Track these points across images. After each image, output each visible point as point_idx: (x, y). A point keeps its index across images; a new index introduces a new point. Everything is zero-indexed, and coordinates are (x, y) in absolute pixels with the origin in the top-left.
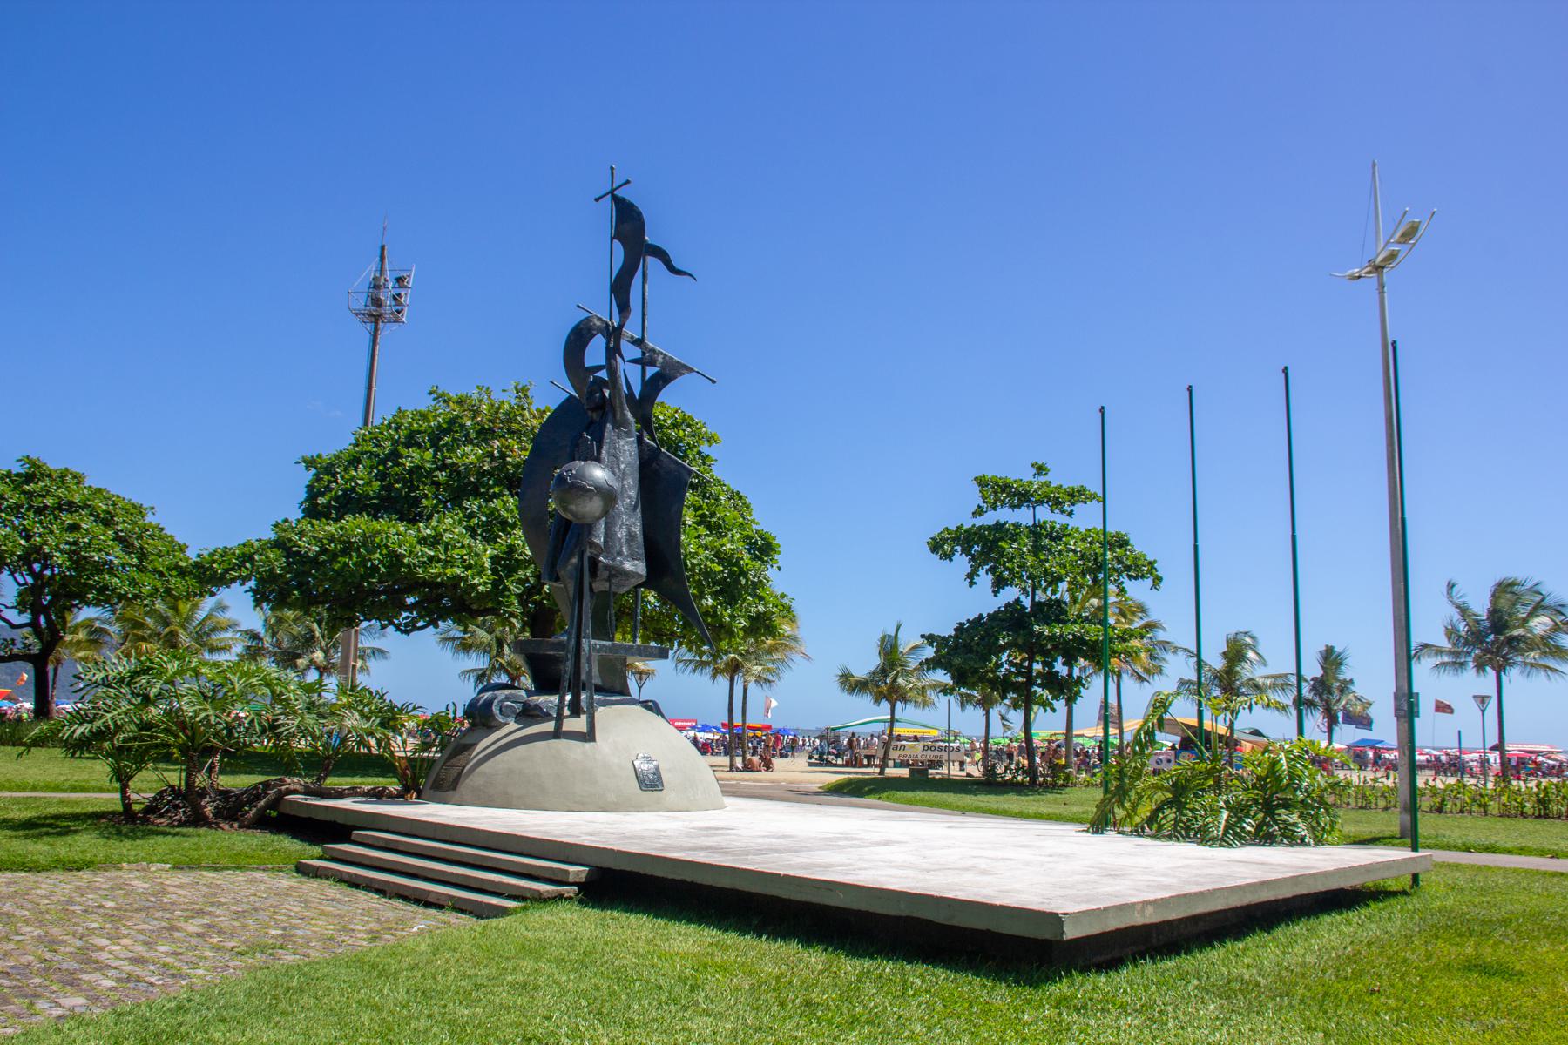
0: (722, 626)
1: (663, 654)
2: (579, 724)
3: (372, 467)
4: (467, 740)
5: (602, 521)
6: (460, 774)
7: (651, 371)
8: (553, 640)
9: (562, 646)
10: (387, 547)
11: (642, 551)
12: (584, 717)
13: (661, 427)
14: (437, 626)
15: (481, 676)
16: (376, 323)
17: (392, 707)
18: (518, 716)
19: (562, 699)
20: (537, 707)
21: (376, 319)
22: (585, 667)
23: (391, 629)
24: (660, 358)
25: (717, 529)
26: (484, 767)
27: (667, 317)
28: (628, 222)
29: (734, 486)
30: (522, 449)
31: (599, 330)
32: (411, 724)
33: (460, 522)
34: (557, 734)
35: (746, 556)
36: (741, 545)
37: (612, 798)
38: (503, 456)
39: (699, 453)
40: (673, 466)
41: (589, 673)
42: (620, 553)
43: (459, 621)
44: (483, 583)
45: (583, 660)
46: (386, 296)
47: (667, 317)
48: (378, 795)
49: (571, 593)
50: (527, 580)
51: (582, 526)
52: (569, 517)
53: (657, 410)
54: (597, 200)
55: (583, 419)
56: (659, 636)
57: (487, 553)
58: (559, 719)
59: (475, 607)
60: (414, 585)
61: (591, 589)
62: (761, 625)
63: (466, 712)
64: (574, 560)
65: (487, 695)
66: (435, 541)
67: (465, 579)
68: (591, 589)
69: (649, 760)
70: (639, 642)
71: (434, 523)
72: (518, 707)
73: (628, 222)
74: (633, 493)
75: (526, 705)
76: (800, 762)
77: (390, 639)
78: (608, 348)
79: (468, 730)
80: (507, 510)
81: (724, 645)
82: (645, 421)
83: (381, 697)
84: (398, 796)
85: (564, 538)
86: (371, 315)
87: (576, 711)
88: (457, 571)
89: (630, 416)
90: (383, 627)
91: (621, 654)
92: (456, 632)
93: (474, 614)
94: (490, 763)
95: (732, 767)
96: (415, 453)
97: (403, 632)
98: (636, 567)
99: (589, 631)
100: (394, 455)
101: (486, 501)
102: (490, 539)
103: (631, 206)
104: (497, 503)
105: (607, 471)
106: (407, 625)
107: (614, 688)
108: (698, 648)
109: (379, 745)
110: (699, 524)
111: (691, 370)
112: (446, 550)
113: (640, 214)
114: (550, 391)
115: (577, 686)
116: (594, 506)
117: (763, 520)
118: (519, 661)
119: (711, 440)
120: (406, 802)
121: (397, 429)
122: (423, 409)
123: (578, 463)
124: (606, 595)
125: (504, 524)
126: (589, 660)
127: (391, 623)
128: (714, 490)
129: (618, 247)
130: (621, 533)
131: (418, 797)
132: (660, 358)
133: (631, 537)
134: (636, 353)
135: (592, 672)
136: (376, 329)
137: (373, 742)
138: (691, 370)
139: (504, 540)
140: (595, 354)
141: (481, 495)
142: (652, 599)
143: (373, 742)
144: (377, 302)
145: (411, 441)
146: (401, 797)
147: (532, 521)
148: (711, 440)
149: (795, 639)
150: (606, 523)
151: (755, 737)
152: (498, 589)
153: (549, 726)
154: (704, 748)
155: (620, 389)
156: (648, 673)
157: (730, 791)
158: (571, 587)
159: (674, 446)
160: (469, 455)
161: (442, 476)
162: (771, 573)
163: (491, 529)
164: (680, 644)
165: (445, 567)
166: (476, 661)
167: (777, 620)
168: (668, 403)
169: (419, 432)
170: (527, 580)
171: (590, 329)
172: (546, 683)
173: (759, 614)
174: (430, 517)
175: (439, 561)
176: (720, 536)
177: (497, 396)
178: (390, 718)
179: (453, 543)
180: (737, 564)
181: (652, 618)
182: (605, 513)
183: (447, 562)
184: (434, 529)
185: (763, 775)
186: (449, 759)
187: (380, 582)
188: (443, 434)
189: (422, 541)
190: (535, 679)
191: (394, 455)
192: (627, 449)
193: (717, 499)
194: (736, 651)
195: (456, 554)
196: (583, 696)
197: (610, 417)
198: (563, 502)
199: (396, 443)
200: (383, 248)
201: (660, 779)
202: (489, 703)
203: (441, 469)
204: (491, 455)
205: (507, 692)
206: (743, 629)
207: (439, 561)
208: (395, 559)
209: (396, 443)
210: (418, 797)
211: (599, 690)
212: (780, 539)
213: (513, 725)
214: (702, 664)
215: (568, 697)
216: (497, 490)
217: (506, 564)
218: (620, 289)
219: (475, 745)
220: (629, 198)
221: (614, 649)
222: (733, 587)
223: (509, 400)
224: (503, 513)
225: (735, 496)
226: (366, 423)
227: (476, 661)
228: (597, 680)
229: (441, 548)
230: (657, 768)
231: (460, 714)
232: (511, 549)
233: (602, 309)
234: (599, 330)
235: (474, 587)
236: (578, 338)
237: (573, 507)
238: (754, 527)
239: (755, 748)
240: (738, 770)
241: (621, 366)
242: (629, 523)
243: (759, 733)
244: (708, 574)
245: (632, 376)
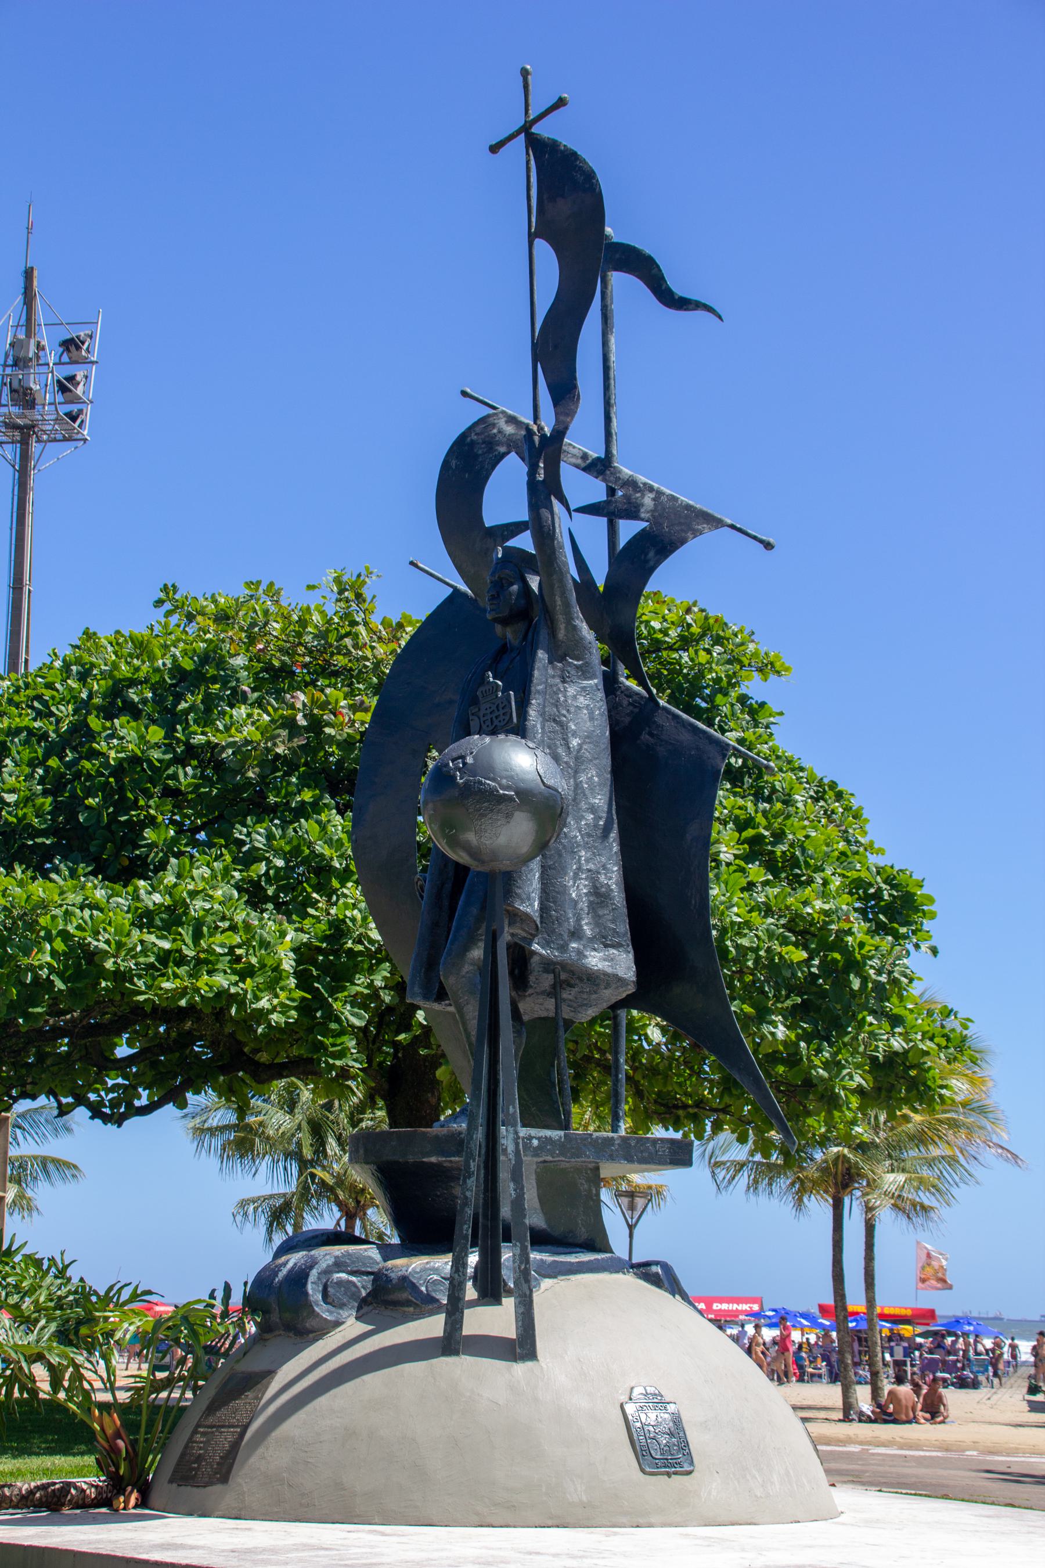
0: (809, 1084)
1: (679, 1155)
2: (496, 1320)
3: (32, 764)
4: (252, 1365)
5: (535, 865)
6: (235, 1446)
7: (628, 530)
8: (435, 1130)
9: (457, 1143)
10: (65, 935)
11: (623, 927)
12: (509, 1303)
13: (657, 646)
14: (182, 1105)
15: (280, 1213)
16: (25, 443)
17: (84, 1294)
18: (363, 1303)
19: (459, 1264)
20: (406, 1282)
21: (25, 434)
22: (507, 1189)
23: (82, 1113)
24: (648, 500)
25: (790, 869)
26: (291, 1426)
27: (662, 405)
28: (565, 195)
29: (823, 769)
30: (354, 708)
31: (512, 445)
32: (128, 1329)
33: (226, 872)
34: (451, 1343)
35: (859, 927)
36: (844, 903)
37: (577, 1492)
38: (316, 725)
39: (743, 699)
40: (685, 737)
41: (518, 1204)
42: (576, 934)
43: (229, 1092)
44: (276, 1006)
45: (504, 1174)
46: (41, 382)
47: (662, 405)
48: (52, 1503)
49: (473, 1024)
50: (375, 994)
51: (489, 878)
52: (462, 857)
53: (646, 607)
54: (494, 149)
55: (484, 645)
56: (669, 1111)
57: (286, 941)
58: (455, 1310)
59: (264, 1057)
60: (131, 1016)
61: (516, 1014)
62: (900, 1081)
63: (247, 1299)
64: (477, 953)
65: (294, 1259)
66: (172, 918)
67: (239, 1000)
68: (516, 1014)
69: (658, 1401)
70: (625, 1126)
71: (170, 879)
72: (363, 1285)
73: (565, 195)
74: (600, 800)
75: (380, 1279)
76: (1008, 1400)
77: (83, 1137)
78: (532, 485)
79: (255, 1341)
80: (329, 842)
81: (816, 1124)
82: (622, 643)
83: (61, 1273)
84: (98, 1503)
85: (453, 902)
86: (16, 427)
87: (491, 1290)
88: (221, 981)
89: (587, 633)
90: (63, 1111)
91: (588, 1158)
92: (224, 1116)
93: (264, 1074)
94: (301, 1415)
95: (849, 1412)
96: (126, 728)
97: (106, 1119)
98: (614, 962)
99: (515, 1109)
100: (80, 735)
101: (285, 824)
102: (294, 908)
103: (570, 159)
104: (308, 827)
105: (543, 755)
106: (114, 1104)
107: (574, 1236)
108: (760, 1132)
109: (56, 1383)
110: (748, 858)
111: (718, 523)
112: (197, 936)
113: (590, 176)
114: (410, 583)
115: (491, 1233)
116: (514, 833)
117: (893, 844)
118: (361, 1176)
119: (767, 668)
120: (117, 1516)
121: (83, 677)
122: (140, 630)
123: (477, 742)
124: (549, 1025)
125: (322, 872)
126: (517, 1176)
127: (81, 1100)
128: (780, 781)
129: (545, 252)
130: (577, 890)
131: (143, 1503)
132: (648, 500)
133: (599, 896)
134: (594, 490)
135: (525, 1200)
136: (25, 457)
137: (40, 1371)
138: (718, 523)
139: (322, 912)
140: (505, 496)
141: (273, 811)
142: (655, 1034)
143: (40, 1371)
144: (25, 398)
145: (116, 703)
146: (102, 1504)
147: (383, 867)
148: (767, 668)
149: (982, 1110)
150: (544, 869)
151: (894, 1337)
152: (314, 1012)
153: (433, 1326)
154: (783, 1364)
155: (562, 573)
156: (651, 1194)
157: (844, 1471)
158: (472, 1011)
159: (688, 690)
160: (244, 724)
161: (186, 776)
162: (917, 961)
163: (290, 889)
164: (717, 1127)
165: (194, 975)
166: (270, 1179)
167: (937, 1064)
168: (672, 594)
169: (132, 683)
170: (375, 995)
171: (490, 443)
172: (424, 1225)
173: (892, 1057)
174: (162, 866)
175: (181, 961)
176: (797, 882)
177: (294, 598)
178: (79, 1322)
179: (210, 919)
180: (839, 945)
181: (653, 1071)
182: (541, 846)
183: (199, 962)
184: (170, 891)
185: (923, 1431)
186: (212, 1408)
187: (54, 1011)
188: (191, 685)
189: (145, 919)
190: (399, 1218)
191: (80, 735)
192: (579, 700)
193: (788, 802)
194: (847, 1139)
195: (219, 943)
196: (507, 1255)
197: (543, 635)
198: (448, 827)
199: (83, 707)
200: (28, 274)
201: (684, 1445)
202: (299, 1277)
203: (180, 761)
204: (289, 723)
205: (338, 1250)
206: (860, 1091)
207: (181, 961)
208: (81, 962)
209: (83, 707)
210: (143, 1503)
211: (540, 1239)
212: (933, 885)
213: (352, 1326)
214: (770, 1172)
215: (473, 1259)
216: (307, 796)
217: (327, 963)
218: (553, 353)
219: (269, 1374)
220: (567, 141)
221: (573, 1146)
222: (832, 994)
223: (324, 607)
224: (321, 848)
225: (825, 791)
226: (13, 664)
227: (270, 1179)
228: (535, 1219)
229: (186, 933)
230: (677, 1420)
231: (237, 1299)
232: (338, 930)
233: (516, 396)
234: (512, 445)
235: (261, 1015)
236: (466, 466)
237: (471, 837)
238: (873, 860)
239: (899, 1364)
240: (863, 1418)
241: (563, 522)
242: (594, 868)
243: (907, 1330)
244: (775, 968)
245: (588, 543)
